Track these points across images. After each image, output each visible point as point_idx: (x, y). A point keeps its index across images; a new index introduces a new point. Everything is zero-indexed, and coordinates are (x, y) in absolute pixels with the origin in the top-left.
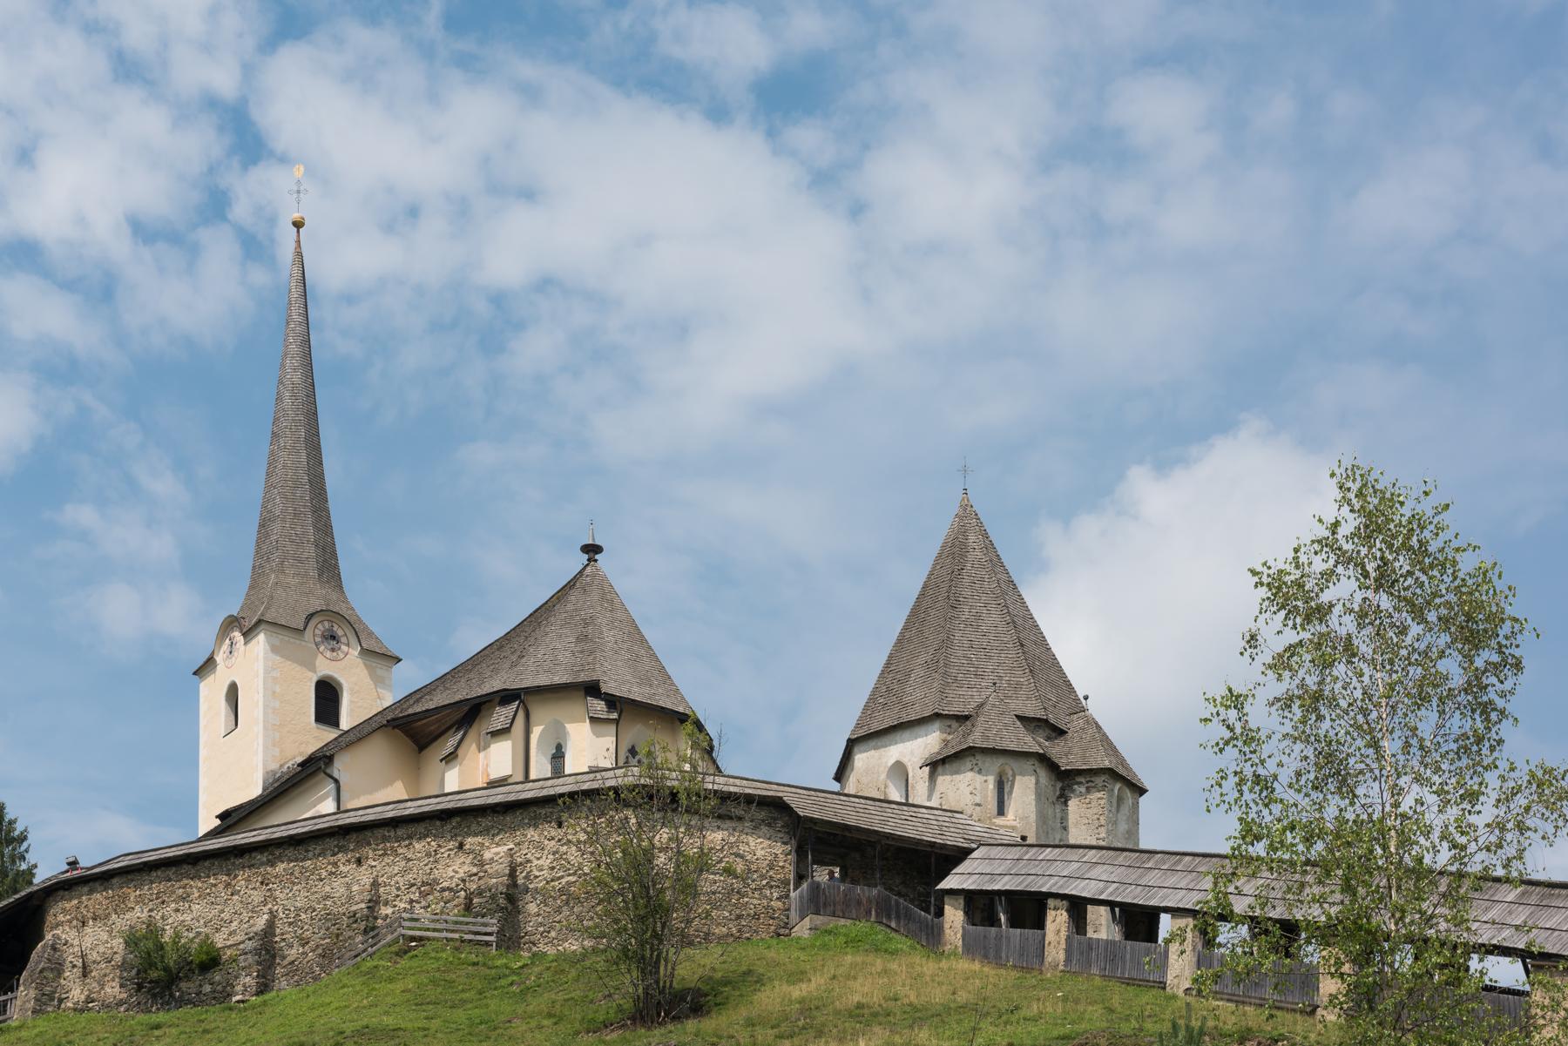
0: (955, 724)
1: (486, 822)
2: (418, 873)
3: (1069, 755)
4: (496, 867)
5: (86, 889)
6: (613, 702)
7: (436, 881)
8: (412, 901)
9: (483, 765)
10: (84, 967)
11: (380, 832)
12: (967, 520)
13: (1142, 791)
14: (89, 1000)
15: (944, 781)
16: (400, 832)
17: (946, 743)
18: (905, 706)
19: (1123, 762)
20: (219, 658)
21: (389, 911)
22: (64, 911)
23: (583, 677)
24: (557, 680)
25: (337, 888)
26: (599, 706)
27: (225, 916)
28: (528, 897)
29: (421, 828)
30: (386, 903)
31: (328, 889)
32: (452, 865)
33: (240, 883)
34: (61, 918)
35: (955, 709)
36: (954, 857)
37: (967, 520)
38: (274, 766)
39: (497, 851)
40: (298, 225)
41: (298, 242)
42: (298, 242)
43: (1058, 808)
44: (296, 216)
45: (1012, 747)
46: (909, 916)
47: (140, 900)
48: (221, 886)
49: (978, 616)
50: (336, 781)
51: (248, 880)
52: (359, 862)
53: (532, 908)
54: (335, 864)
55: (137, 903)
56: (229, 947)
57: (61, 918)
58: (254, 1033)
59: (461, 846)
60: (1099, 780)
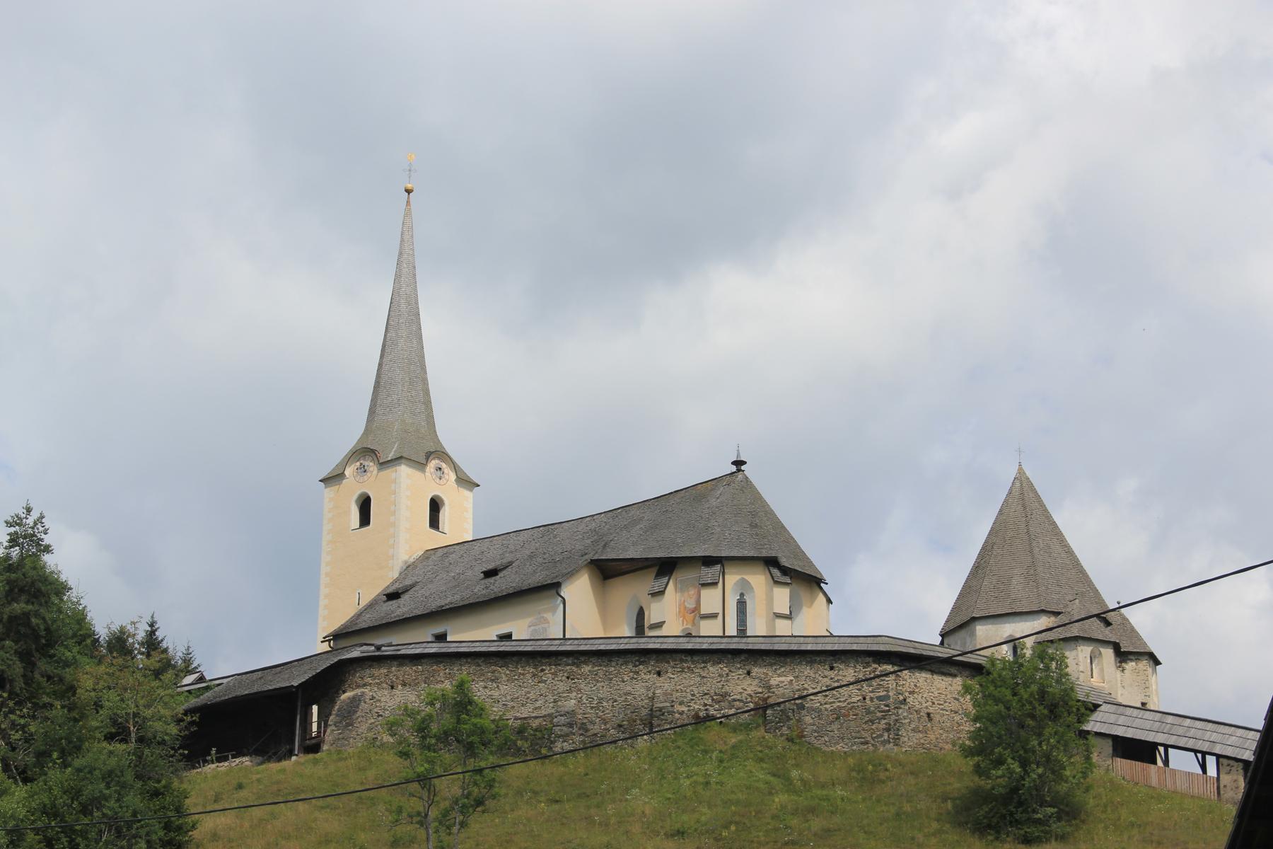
1: (768, 660)
2: (713, 685)
5: (621, 661)
6: (785, 571)
8: (705, 705)
9: (670, 613)
11: (679, 656)
16: (696, 658)
19: (789, 541)
21: (685, 709)
22: (372, 676)
23: (764, 554)
24: (746, 553)
26: (776, 572)
27: (532, 696)
28: (804, 712)
29: (715, 657)
30: (681, 703)
31: (629, 688)
32: (743, 685)
33: (548, 676)
34: (369, 680)
40: (409, 191)
44: (409, 186)
48: (528, 676)
51: (555, 674)
52: (659, 674)
53: (808, 719)
55: (446, 678)
56: (536, 717)
57: (369, 680)
58: (767, 736)
59: (749, 673)
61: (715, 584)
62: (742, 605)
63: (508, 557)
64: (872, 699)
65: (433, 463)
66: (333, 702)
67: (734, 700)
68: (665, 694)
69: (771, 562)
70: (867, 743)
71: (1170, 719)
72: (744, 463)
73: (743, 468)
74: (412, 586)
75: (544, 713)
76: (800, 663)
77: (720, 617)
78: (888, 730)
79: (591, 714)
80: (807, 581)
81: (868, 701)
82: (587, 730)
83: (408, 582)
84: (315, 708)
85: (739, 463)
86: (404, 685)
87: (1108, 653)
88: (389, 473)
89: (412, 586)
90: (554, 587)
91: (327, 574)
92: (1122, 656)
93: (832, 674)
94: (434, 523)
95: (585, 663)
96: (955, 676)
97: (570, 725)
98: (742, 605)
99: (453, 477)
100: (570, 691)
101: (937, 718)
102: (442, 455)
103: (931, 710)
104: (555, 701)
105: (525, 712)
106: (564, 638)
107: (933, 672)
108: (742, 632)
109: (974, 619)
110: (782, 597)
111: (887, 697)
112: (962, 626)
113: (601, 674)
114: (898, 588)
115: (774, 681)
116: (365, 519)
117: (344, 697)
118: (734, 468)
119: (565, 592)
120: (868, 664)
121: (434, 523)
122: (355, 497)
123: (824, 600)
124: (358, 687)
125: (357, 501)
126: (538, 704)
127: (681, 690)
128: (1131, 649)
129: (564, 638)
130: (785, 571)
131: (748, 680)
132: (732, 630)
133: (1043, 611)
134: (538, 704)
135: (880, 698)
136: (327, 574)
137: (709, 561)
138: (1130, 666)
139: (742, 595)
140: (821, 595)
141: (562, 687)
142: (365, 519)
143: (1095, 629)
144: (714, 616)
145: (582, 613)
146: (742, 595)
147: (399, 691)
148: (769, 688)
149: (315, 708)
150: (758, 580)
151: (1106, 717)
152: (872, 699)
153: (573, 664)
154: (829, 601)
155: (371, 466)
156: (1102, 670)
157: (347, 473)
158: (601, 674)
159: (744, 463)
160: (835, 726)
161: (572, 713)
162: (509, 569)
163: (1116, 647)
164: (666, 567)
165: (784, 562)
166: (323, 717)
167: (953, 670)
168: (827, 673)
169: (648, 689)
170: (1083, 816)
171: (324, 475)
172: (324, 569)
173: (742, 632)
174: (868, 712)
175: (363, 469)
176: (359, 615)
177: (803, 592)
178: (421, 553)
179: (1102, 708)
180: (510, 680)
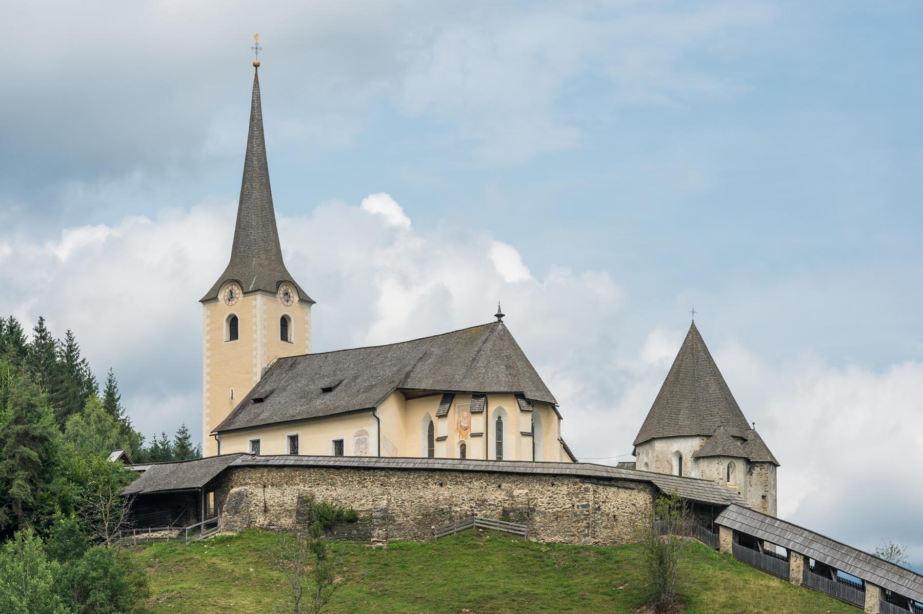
0: (705, 439)
2: (476, 494)
3: (754, 457)
4: (520, 499)
5: (416, 475)
6: (530, 402)
7: (485, 500)
10: (265, 507)
12: (693, 325)
13: (775, 465)
14: (270, 524)
15: (703, 464)
16: (465, 475)
17: (702, 447)
18: (680, 427)
20: (221, 297)
21: (458, 509)
24: (502, 389)
25: (429, 494)
26: (523, 403)
28: (535, 514)
29: (478, 475)
30: (456, 505)
31: (422, 494)
32: (496, 495)
35: (706, 433)
36: (719, 509)
37: (693, 325)
38: (265, 365)
39: (521, 492)
40: (256, 66)
41: (256, 75)
42: (256, 75)
43: (748, 476)
45: (735, 455)
46: (704, 533)
47: (304, 481)
48: (355, 483)
49: (707, 386)
50: (378, 419)
52: (441, 485)
53: (538, 519)
54: (427, 484)
59: (500, 486)
60: (766, 466)
61: (481, 412)
62: (499, 424)
63: (339, 377)
64: (578, 507)
65: (282, 290)
66: (226, 493)
67: (490, 505)
68: (445, 499)
69: (519, 395)
70: (574, 535)
71: (768, 520)
72: (503, 315)
73: (502, 319)
74: (272, 392)
75: (366, 508)
76: (532, 482)
77: (484, 435)
78: (588, 528)
79: (397, 510)
80: (541, 405)
81: (576, 508)
82: (395, 521)
83: (268, 388)
84: (212, 495)
85: (500, 316)
86: (273, 485)
87: (740, 467)
88: (250, 298)
89: (272, 392)
90: (373, 409)
91: (208, 374)
92: (750, 464)
93: (553, 489)
94: (284, 336)
95: (393, 475)
96: (633, 489)
97: (383, 518)
98: (499, 424)
99: (296, 299)
100: (383, 494)
101: (620, 518)
102: (292, 283)
103: (616, 513)
104: (373, 501)
105: (355, 506)
106: (379, 457)
107: (618, 487)
108: (499, 459)
109: (654, 439)
110: (525, 422)
111: (588, 506)
112: (647, 442)
113: (403, 483)
114: (600, 427)
115: (515, 494)
116: (234, 335)
117: (233, 491)
118: (496, 319)
119: (379, 413)
120: (576, 483)
121: (284, 336)
122: (226, 317)
123: (556, 417)
124: (241, 485)
125: (227, 319)
126: (362, 502)
127: (460, 497)
128: (757, 459)
129: (379, 457)
130: (530, 402)
131: (499, 492)
132: (492, 456)
133: (698, 435)
134: (362, 502)
135: (583, 506)
136: (208, 374)
137: (477, 395)
138: (757, 470)
139: (499, 418)
140: (554, 413)
141: (378, 491)
142: (234, 335)
143: (737, 448)
144: (480, 435)
145: (394, 434)
146: (499, 418)
147: (269, 489)
148: (513, 497)
149: (212, 495)
150: (511, 410)
151: (733, 516)
152: (578, 507)
153: (385, 476)
154: (560, 418)
155: (237, 290)
156: (735, 476)
157: (220, 297)
158: (403, 483)
159: (503, 315)
160: (555, 524)
161: (385, 510)
162: (340, 387)
163: (748, 461)
164: (448, 397)
165: (529, 395)
166: (219, 503)
167: (632, 485)
168: (550, 488)
169: (434, 495)
170: (694, 600)
171: (202, 295)
172: (206, 370)
173: (499, 459)
174: (576, 515)
175: (231, 297)
176: (235, 414)
177: (542, 414)
178: (275, 361)
179: (731, 508)
180: (343, 485)
